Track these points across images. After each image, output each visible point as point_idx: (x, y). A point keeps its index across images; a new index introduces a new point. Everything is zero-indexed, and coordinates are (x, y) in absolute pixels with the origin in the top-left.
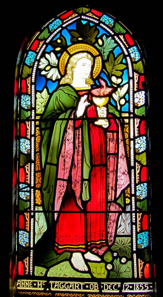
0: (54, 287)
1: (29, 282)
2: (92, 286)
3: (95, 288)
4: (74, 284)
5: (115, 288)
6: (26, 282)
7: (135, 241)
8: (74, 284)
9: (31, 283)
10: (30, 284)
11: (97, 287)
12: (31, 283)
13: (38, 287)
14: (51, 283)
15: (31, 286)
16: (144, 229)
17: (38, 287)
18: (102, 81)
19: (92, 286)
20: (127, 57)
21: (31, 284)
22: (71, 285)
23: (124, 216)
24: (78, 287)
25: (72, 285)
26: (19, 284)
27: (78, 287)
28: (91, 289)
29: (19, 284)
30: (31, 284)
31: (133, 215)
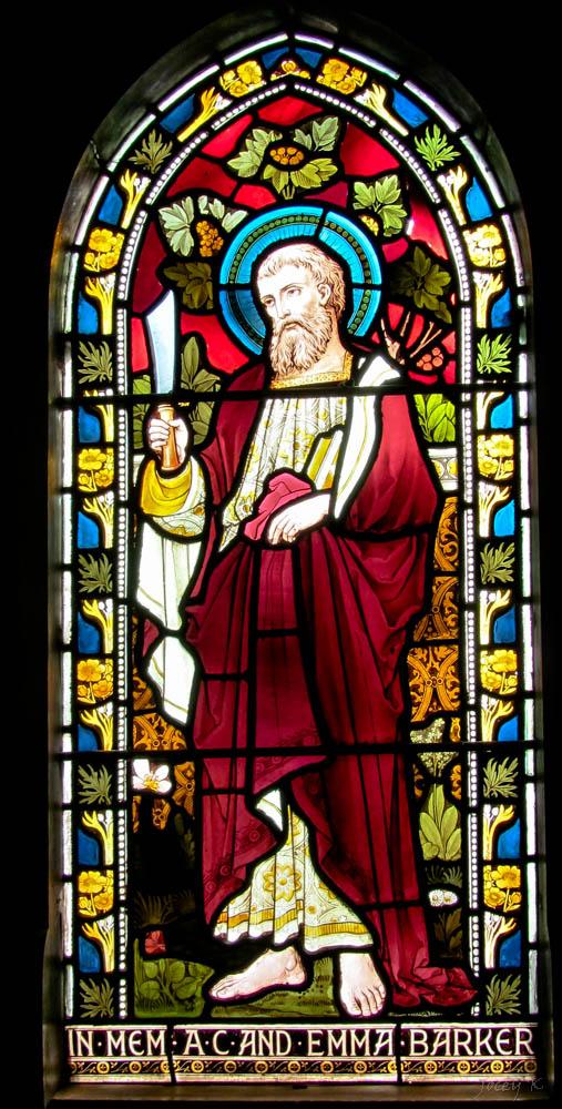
0: (239, 1050)
1: (128, 1033)
2: (284, 1048)
3: (310, 1048)
4: (452, 1034)
5: (222, 1048)
6: (261, 1033)
7: (469, 359)
8: (452, 1034)
9: (136, 1038)
10: (131, 1043)
11: (423, 1042)
12: (136, 1038)
13: (110, 1052)
14: (188, 1035)
15: (136, 1047)
16: (314, 65)
17: (110, 1052)
18: (71, 361)
19: (284, 1048)
20: (439, 212)
21: (138, 1042)
22: (381, 1038)
23: (241, 438)
24: (465, 1044)
25: (444, 1036)
26: (250, 1046)
27: (465, 1044)
28: (217, 1051)
29: (250, 1046)
30: (138, 1042)
31: (124, 292)
